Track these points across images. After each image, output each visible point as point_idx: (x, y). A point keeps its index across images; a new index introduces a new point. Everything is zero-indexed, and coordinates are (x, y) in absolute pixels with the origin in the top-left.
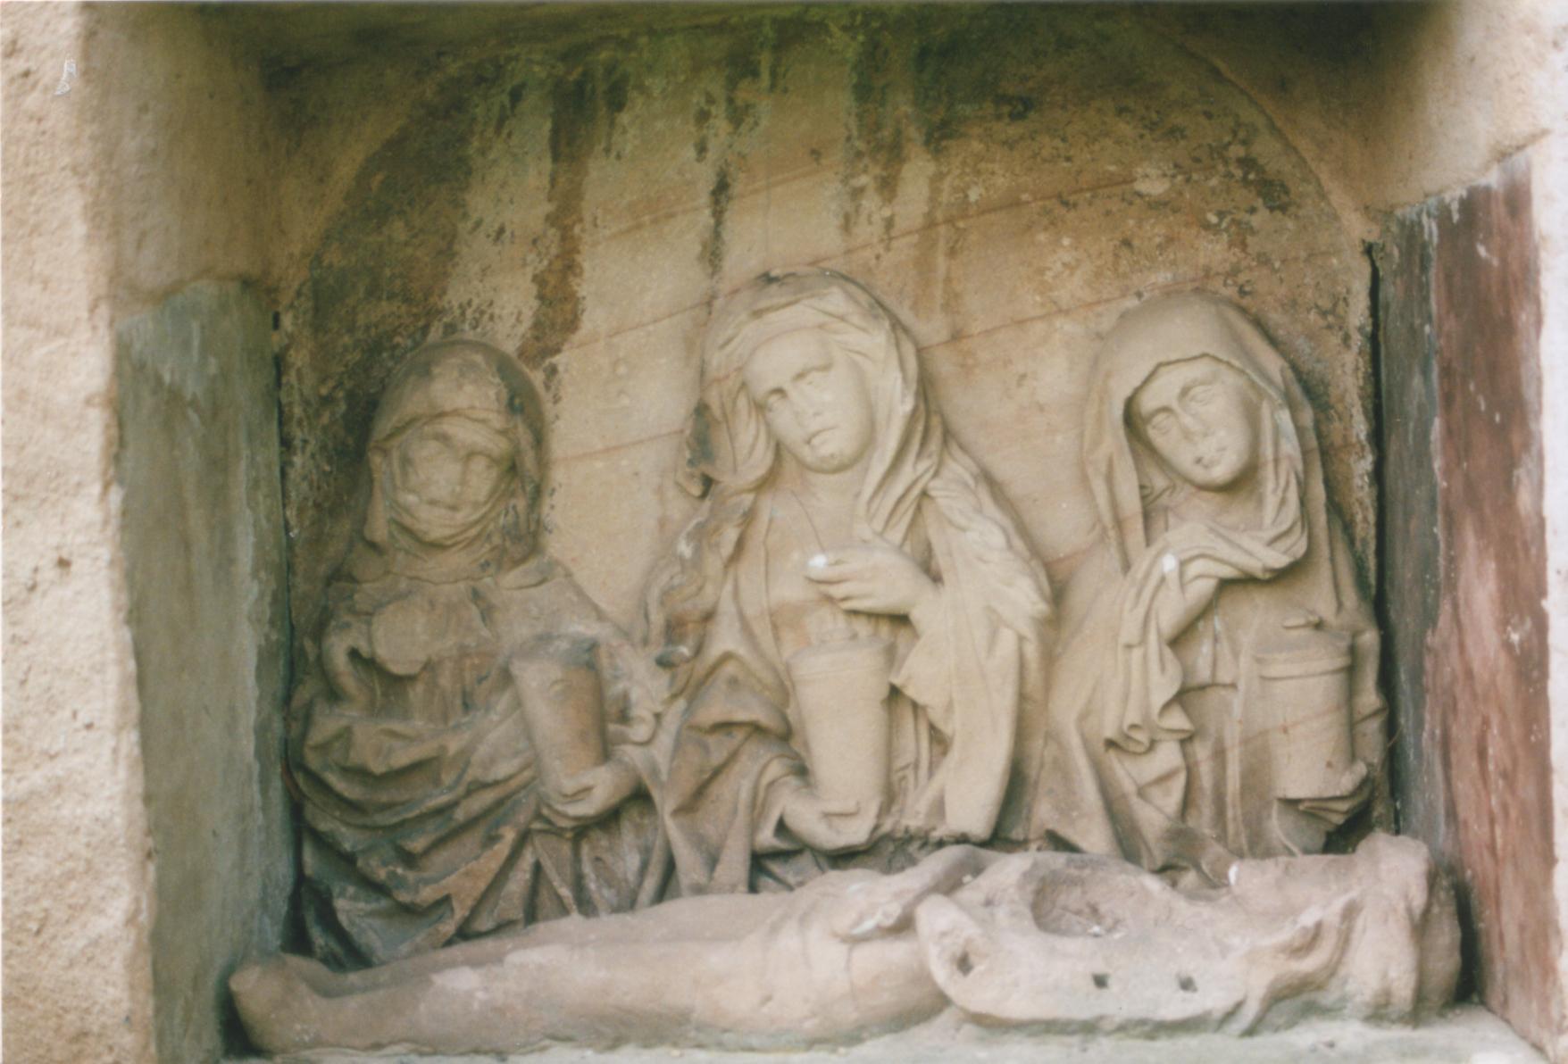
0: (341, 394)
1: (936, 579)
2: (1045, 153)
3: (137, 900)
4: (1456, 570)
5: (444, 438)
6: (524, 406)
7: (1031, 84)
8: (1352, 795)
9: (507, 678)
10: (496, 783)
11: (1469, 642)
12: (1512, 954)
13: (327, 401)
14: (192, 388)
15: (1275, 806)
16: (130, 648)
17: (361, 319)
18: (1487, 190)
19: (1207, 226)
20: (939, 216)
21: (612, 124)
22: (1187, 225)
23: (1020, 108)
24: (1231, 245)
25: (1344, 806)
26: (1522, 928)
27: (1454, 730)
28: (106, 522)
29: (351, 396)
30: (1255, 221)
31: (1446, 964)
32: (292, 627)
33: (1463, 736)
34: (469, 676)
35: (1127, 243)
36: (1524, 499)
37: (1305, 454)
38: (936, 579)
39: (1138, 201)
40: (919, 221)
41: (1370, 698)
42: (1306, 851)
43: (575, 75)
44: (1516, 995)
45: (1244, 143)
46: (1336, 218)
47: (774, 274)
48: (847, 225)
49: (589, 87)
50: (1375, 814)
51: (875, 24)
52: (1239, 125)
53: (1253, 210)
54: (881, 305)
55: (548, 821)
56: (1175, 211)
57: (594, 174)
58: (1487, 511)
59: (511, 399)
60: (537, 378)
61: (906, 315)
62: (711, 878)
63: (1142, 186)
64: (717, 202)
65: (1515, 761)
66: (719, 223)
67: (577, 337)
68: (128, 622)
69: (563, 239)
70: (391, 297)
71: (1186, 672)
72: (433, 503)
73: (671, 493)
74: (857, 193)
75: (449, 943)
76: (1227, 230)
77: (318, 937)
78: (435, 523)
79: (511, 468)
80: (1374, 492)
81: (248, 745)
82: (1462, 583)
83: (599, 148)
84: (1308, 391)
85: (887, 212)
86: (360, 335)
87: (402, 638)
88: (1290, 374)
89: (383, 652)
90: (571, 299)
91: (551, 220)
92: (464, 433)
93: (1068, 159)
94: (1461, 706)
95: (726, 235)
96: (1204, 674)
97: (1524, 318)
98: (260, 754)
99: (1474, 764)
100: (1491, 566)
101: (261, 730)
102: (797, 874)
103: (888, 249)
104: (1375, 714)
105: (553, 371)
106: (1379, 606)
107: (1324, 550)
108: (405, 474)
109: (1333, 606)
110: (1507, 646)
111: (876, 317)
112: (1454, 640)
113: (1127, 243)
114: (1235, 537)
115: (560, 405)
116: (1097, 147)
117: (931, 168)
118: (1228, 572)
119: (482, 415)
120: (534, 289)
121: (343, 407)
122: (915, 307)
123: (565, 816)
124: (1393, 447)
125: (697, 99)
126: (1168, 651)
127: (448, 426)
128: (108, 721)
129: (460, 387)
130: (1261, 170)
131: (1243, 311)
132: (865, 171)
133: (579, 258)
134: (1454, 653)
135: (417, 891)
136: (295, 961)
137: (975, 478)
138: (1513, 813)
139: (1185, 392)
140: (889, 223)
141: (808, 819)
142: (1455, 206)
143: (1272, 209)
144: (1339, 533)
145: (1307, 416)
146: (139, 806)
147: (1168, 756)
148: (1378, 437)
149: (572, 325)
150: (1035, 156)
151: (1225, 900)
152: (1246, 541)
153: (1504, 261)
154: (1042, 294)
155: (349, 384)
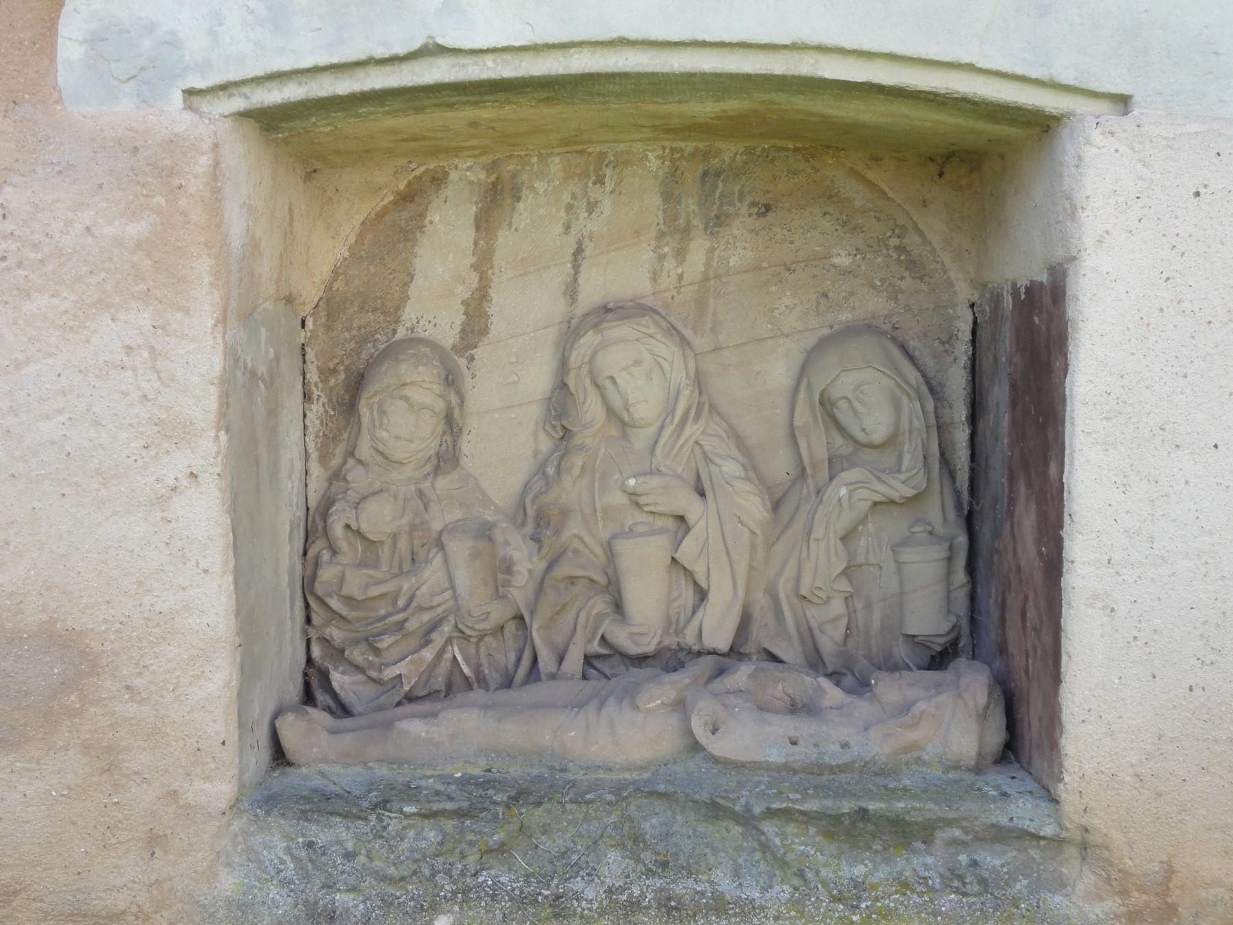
0: (342, 368)
1: (702, 494)
2: (778, 237)
3: (231, 674)
4: (1014, 505)
5: (406, 399)
6: (451, 380)
7: (770, 195)
8: (948, 633)
9: (440, 545)
10: (432, 608)
11: (1020, 551)
12: (1034, 733)
13: (334, 371)
14: (262, 369)
15: (901, 639)
16: (230, 527)
17: (356, 323)
18: (1041, 283)
19: (874, 287)
20: (711, 274)
21: (513, 209)
22: (862, 285)
23: (763, 210)
24: (889, 298)
25: (942, 640)
26: (1040, 719)
27: (1008, 601)
28: (218, 453)
29: (347, 370)
30: (903, 284)
31: (996, 736)
32: (308, 509)
33: (1013, 603)
34: (417, 543)
35: (825, 295)
36: (1053, 470)
37: (928, 427)
38: (702, 494)
39: (833, 270)
40: (699, 277)
41: (960, 577)
42: (920, 668)
43: (492, 179)
44: (1036, 755)
45: (899, 237)
46: (952, 285)
47: (611, 305)
48: (655, 277)
49: (499, 187)
50: (961, 645)
51: (677, 156)
52: (896, 226)
53: (902, 278)
54: (674, 328)
55: (462, 632)
56: (856, 277)
57: (501, 239)
58: (1033, 473)
59: (447, 378)
60: (462, 362)
61: (688, 333)
62: (559, 669)
63: (836, 261)
64: (576, 260)
65: (1041, 622)
66: (576, 273)
67: (485, 339)
68: (228, 512)
69: (481, 279)
70: (375, 310)
71: (851, 556)
72: (397, 437)
73: (542, 435)
74: (661, 258)
75: (399, 704)
76: (886, 290)
77: (320, 696)
78: (399, 451)
79: (449, 419)
80: (969, 452)
81: (285, 579)
82: (1016, 513)
83: (505, 225)
84: (931, 390)
85: (680, 271)
86: (355, 332)
87: (379, 518)
88: (921, 379)
89: (364, 527)
90: (485, 315)
91: (474, 267)
92: (417, 395)
93: (791, 242)
94: (1013, 586)
95: (581, 281)
96: (861, 559)
97: (1057, 364)
98: (291, 585)
99: (1019, 622)
100: (1033, 506)
101: (291, 572)
102: (612, 668)
103: (679, 293)
104: (963, 586)
105: (472, 358)
106: (970, 522)
107: (937, 486)
108: (381, 419)
109: (941, 519)
110: (1040, 553)
111: (672, 335)
112: (1010, 548)
113: (825, 295)
114: (883, 476)
115: (476, 379)
116: (809, 235)
117: (708, 244)
118: (878, 498)
119: (429, 386)
120: (462, 309)
121: (342, 376)
122: (694, 329)
123: (473, 629)
124: (981, 425)
125: (566, 198)
126: (839, 542)
127: (408, 391)
128: (216, 569)
129: (417, 368)
130: (908, 253)
131: (894, 339)
132: (667, 244)
133: (490, 291)
134: (1010, 555)
135: (380, 671)
136: (310, 709)
137: (726, 432)
138: (1039, 652)
139: (857, 387)
140: (681, 277)
141: (622, 638)
142: (1023, 290)
143: (914, 278)
144: (946, 476)
145: (930, 405)
146: (233, 620)
147: (838, 607)
148: (973, 419)
149: (485, 331)
150: (771, 239)
151: (868, 695)
152: (890, 480)
153: (1048, 330)
154: (772, 324)
155: (347, 362)
